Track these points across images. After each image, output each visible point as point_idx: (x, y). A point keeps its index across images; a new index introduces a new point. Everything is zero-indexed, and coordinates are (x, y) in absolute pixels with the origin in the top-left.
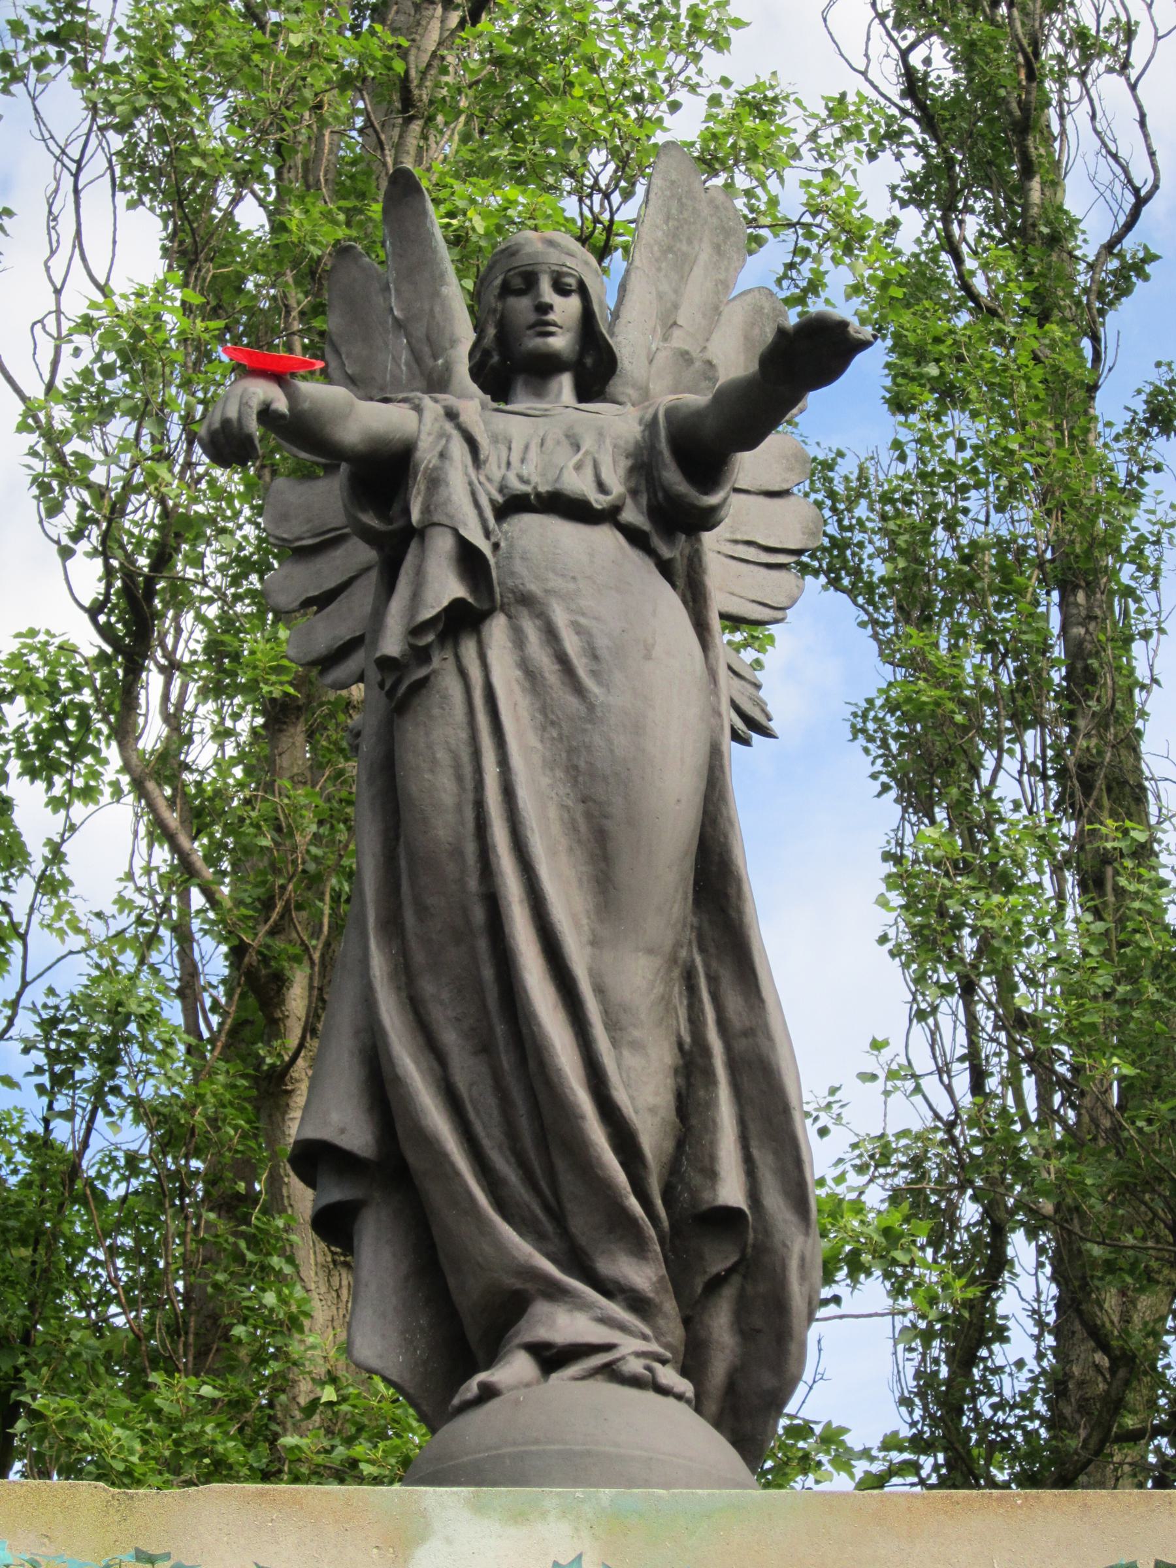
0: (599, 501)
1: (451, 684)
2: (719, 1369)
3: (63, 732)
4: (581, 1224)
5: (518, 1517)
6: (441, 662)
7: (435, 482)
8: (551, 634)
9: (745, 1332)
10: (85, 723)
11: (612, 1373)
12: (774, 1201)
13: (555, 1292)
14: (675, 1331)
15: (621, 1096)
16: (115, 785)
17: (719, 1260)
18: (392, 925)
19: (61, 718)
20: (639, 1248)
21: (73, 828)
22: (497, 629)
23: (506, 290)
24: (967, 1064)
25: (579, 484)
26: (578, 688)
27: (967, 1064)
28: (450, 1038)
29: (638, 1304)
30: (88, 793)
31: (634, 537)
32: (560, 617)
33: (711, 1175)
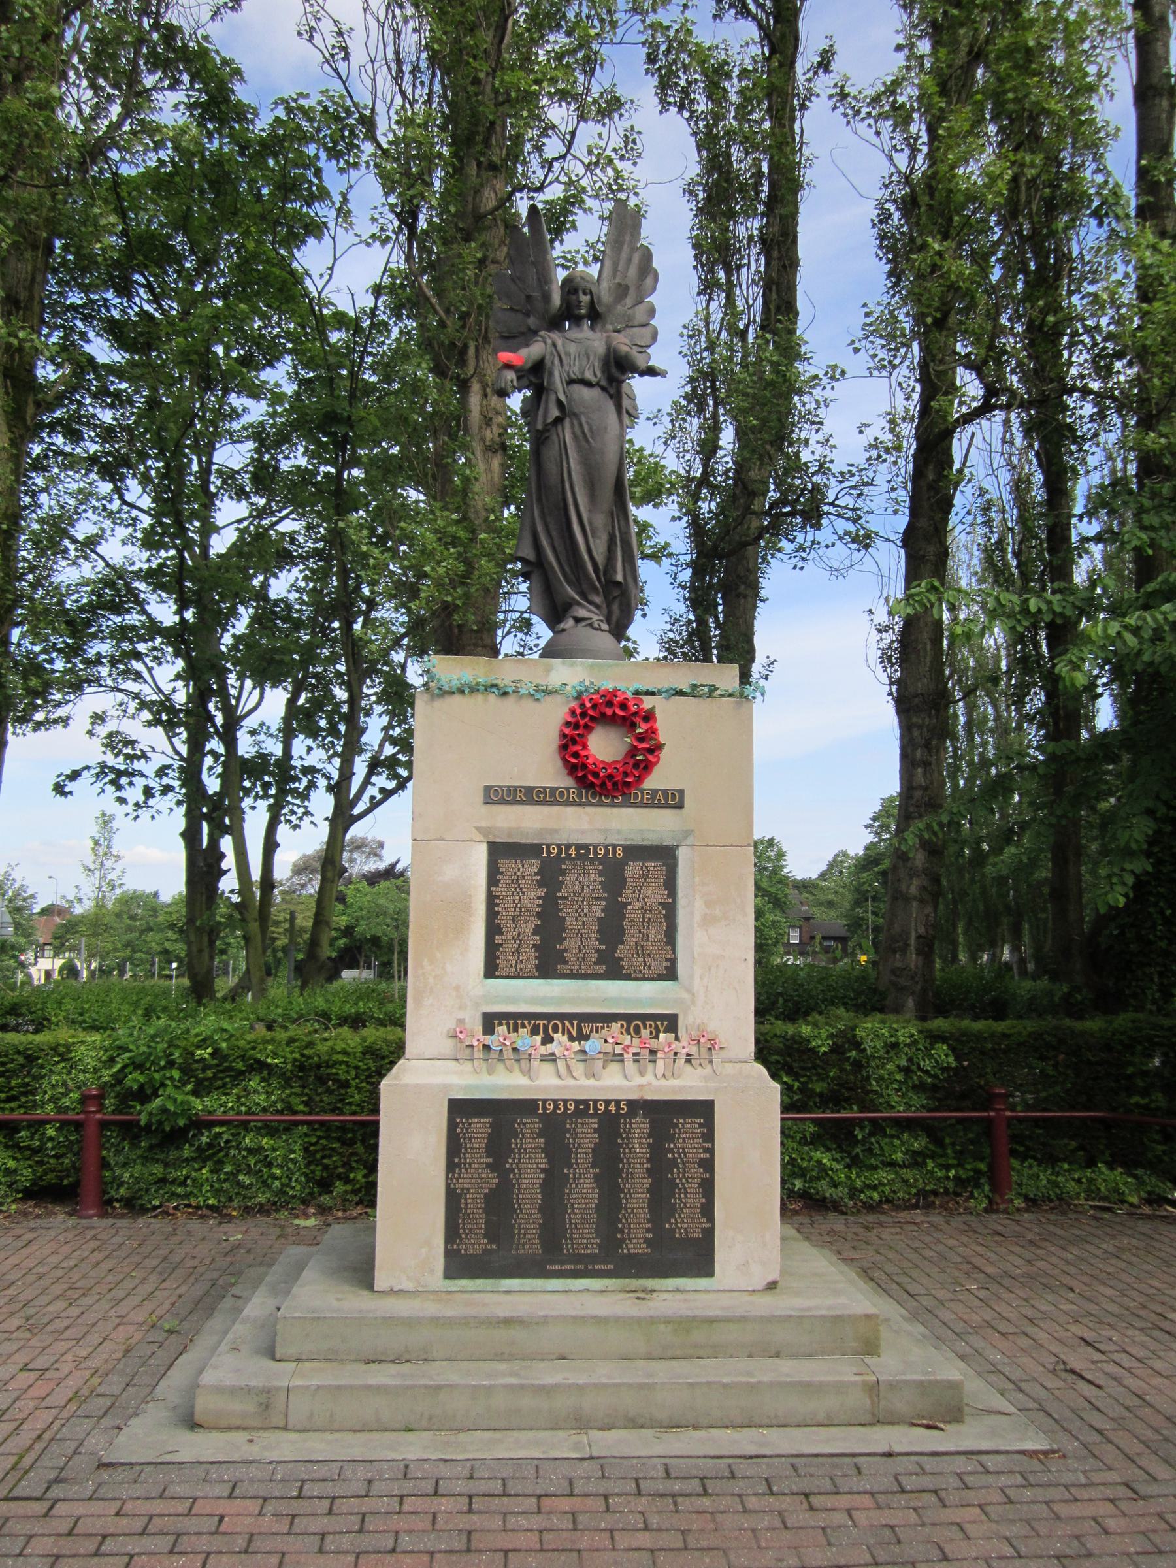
0: (594, 380)
1: (555, 437)
2: (614, 618)
3: (343, 137)
4: (585, 586)
5: (572, 665)
6: (553, 430)
7: (551, 374)
8: (581, 425)
9: (622, 611)
10: (352, 132)
11: (591, 625)
12: (630, 580)
13: (579, 604)
14: (605, 610)
15: (595, 554)
16: (367, 162)
17: (616, 593)
18: (539, 500)
19: (342, 130)
20: (598, 593)
21: (351, 187)
22: (567, 422)
23: (569, 292)
24: (542, 1176)
25: (589, 375)
26: (587, 441)
27: (542, 1176)
28: (554, 534)
29: (597, 606)
30: (356, 166)
31: (603, 389)
32: (583, 419)
33: (615, 572)
